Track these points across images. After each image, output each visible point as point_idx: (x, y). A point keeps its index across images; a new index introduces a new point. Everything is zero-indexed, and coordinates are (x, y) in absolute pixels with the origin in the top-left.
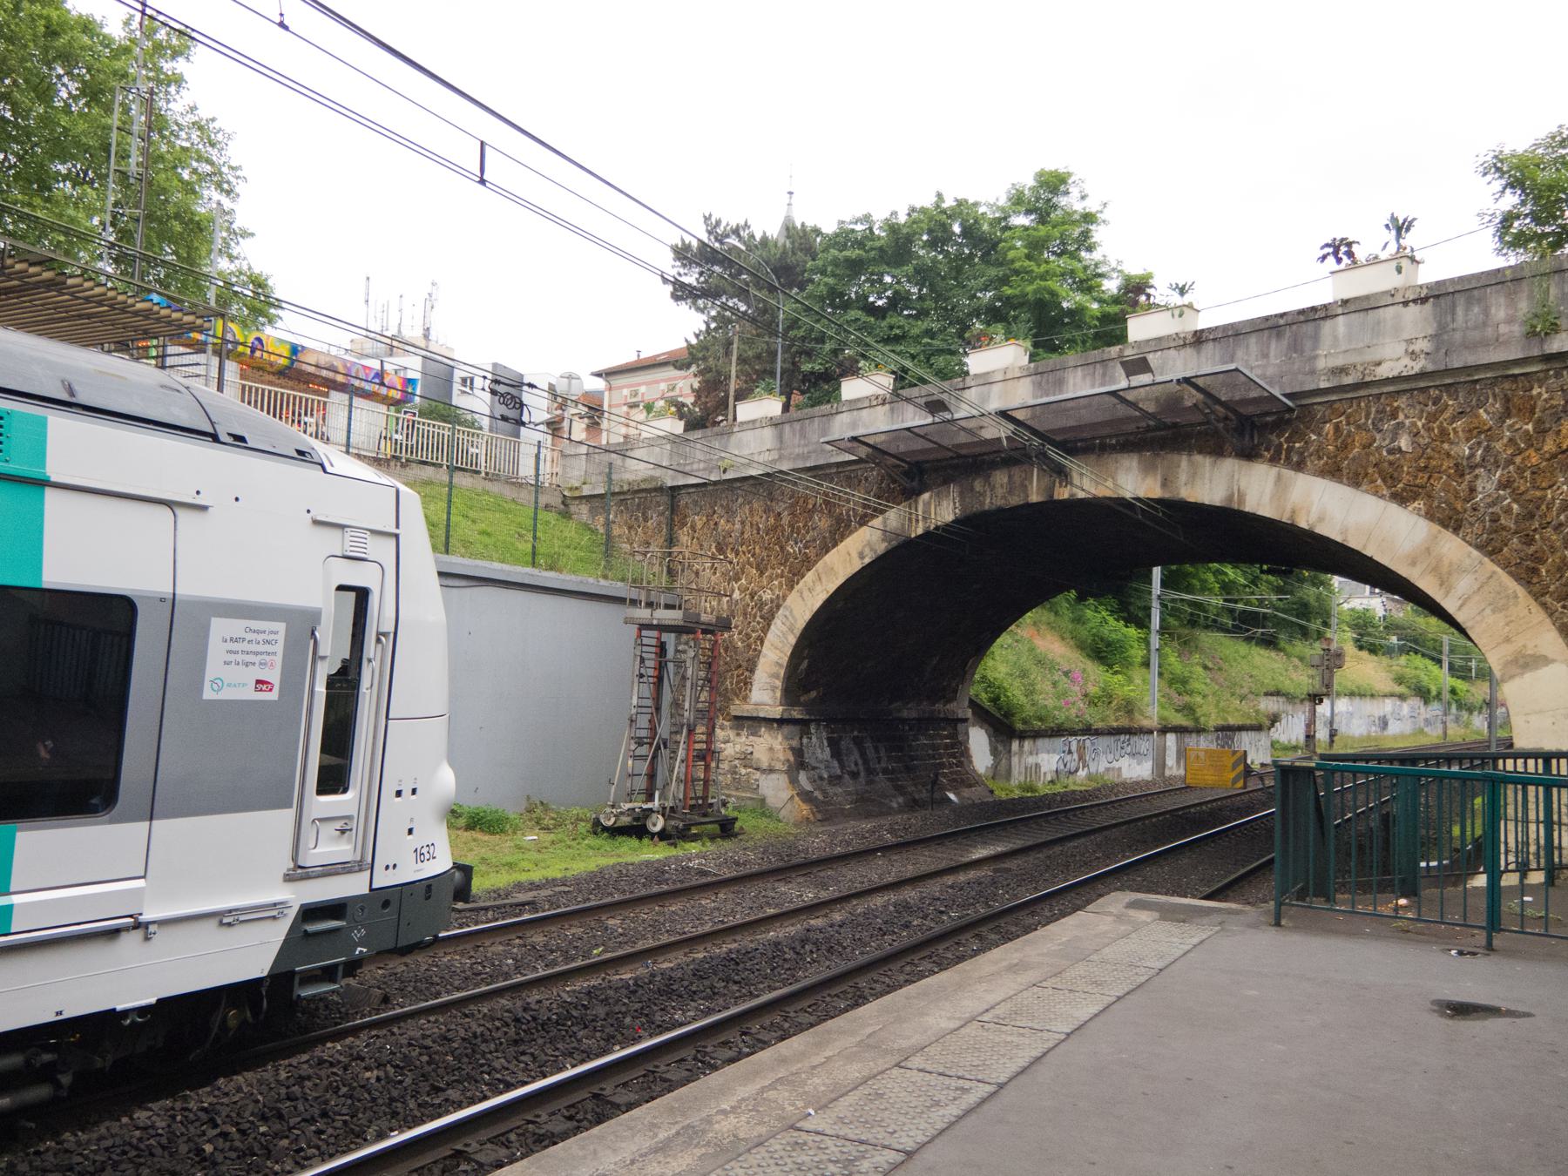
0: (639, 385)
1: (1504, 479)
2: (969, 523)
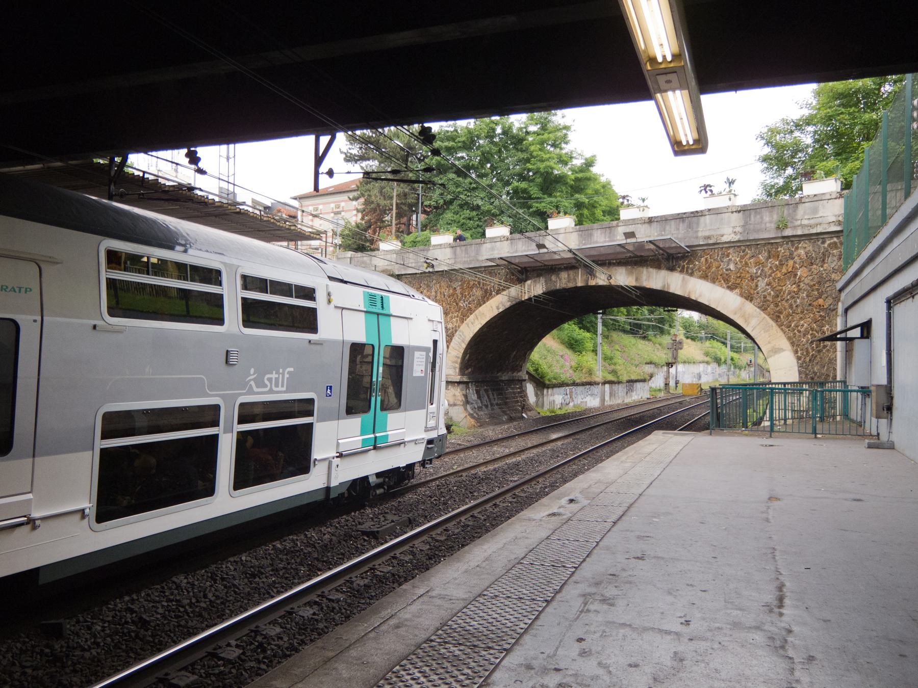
0: (319, 204)
2: (549, 294)
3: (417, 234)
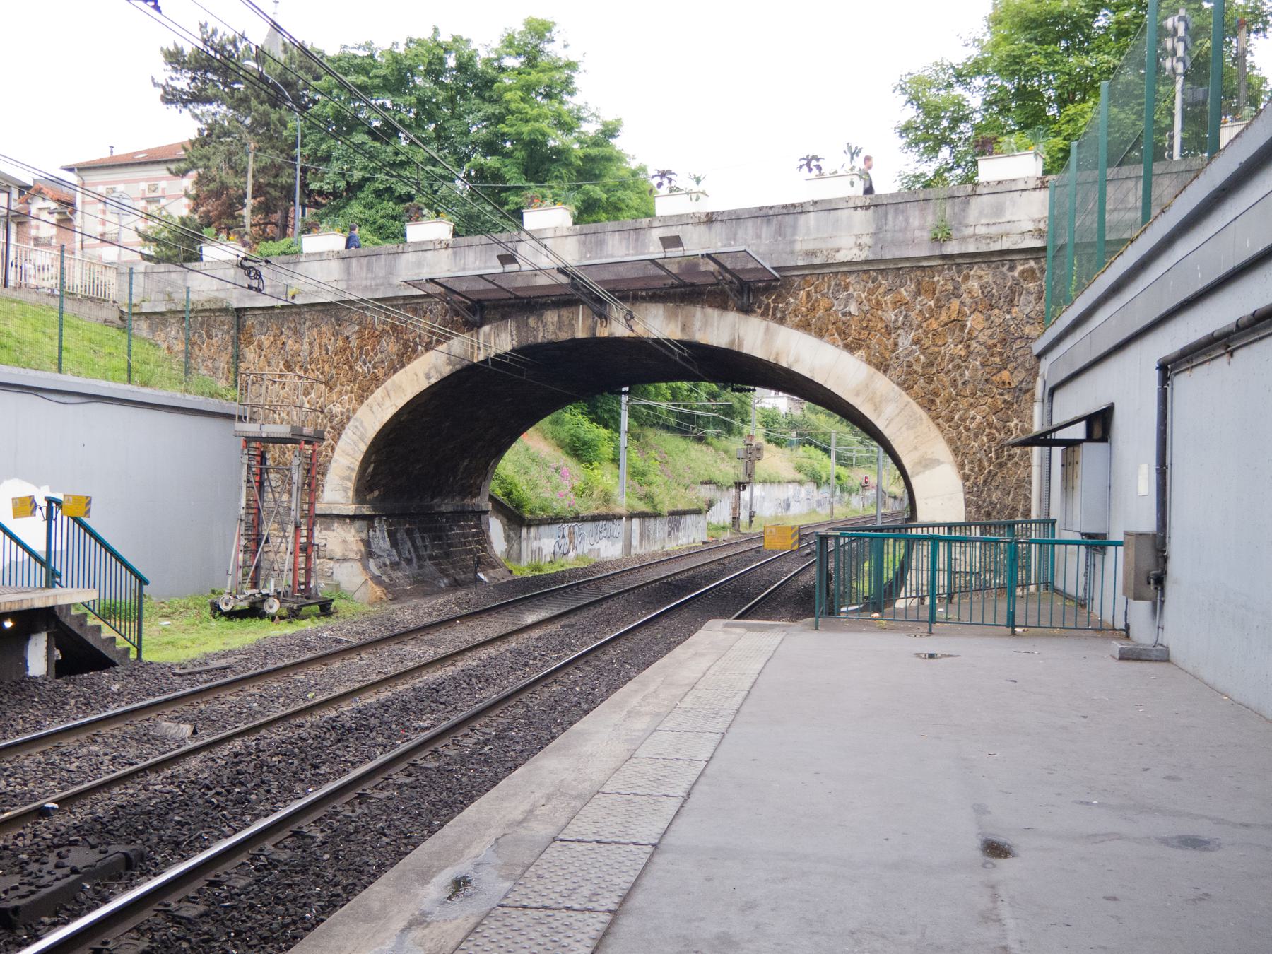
0: (117, 182)
1: (916, 338)
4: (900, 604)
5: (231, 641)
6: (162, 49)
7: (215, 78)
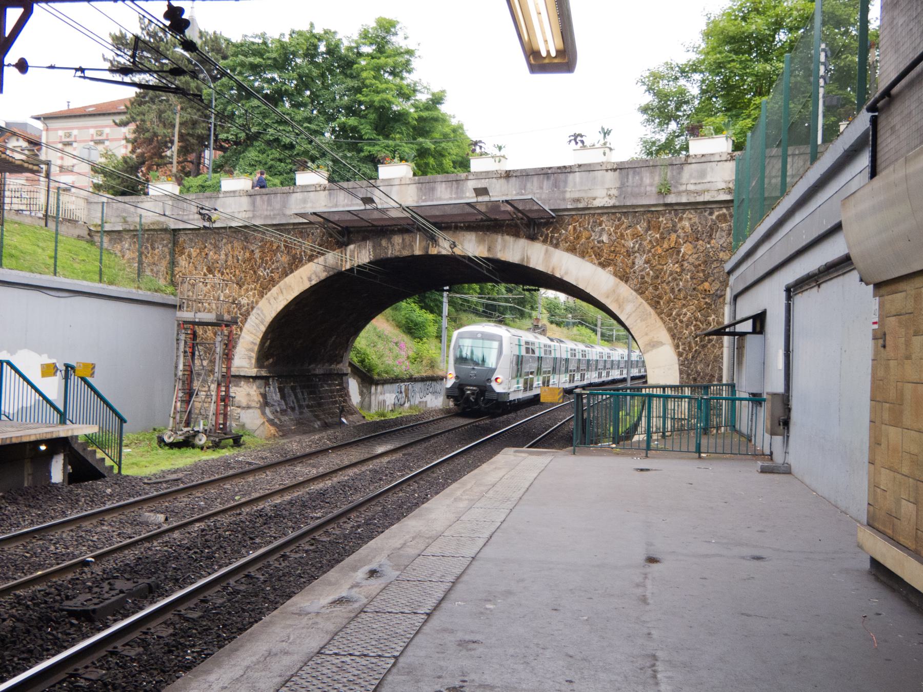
0: (72, 128)
3: (207, 176)
4: (636, 438)
5: (177, 463)
6: (110, 34)
7: (149, 55)
